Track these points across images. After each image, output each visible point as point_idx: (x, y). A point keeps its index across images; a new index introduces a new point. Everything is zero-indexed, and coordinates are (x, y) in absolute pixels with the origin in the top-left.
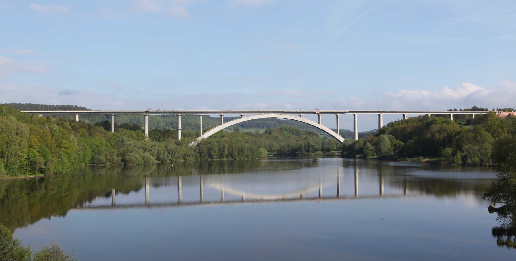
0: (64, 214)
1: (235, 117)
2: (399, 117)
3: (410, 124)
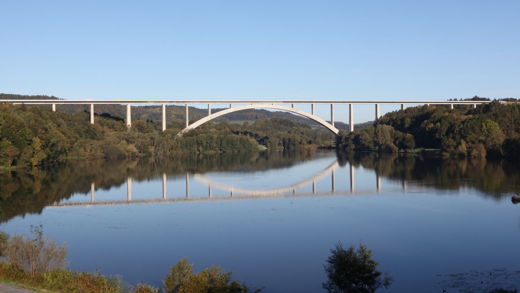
0: (40, 212)
1: (221, 109)
2: (397, 108)
3: (409, 114)
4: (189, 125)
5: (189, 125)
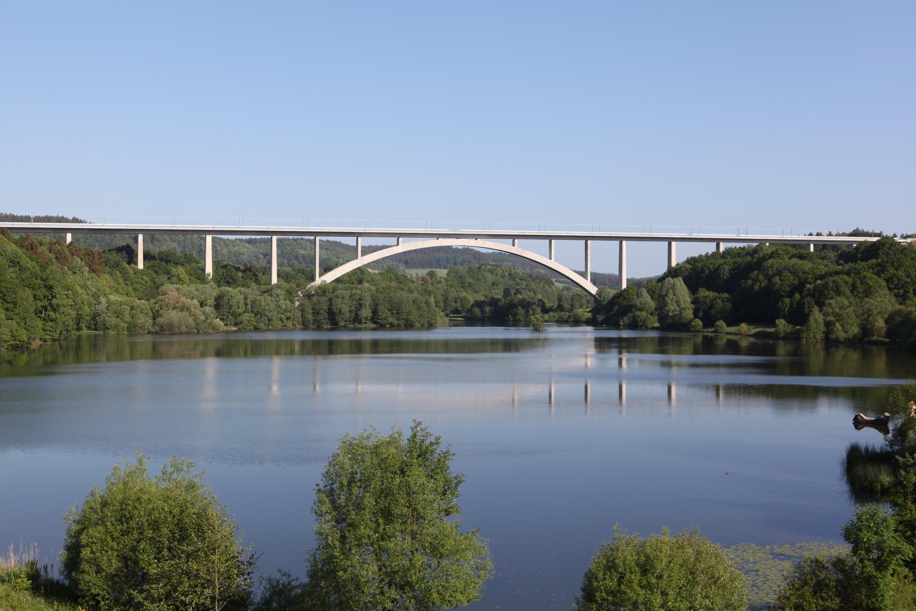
4: (321, 275)
5: (321, 275)
